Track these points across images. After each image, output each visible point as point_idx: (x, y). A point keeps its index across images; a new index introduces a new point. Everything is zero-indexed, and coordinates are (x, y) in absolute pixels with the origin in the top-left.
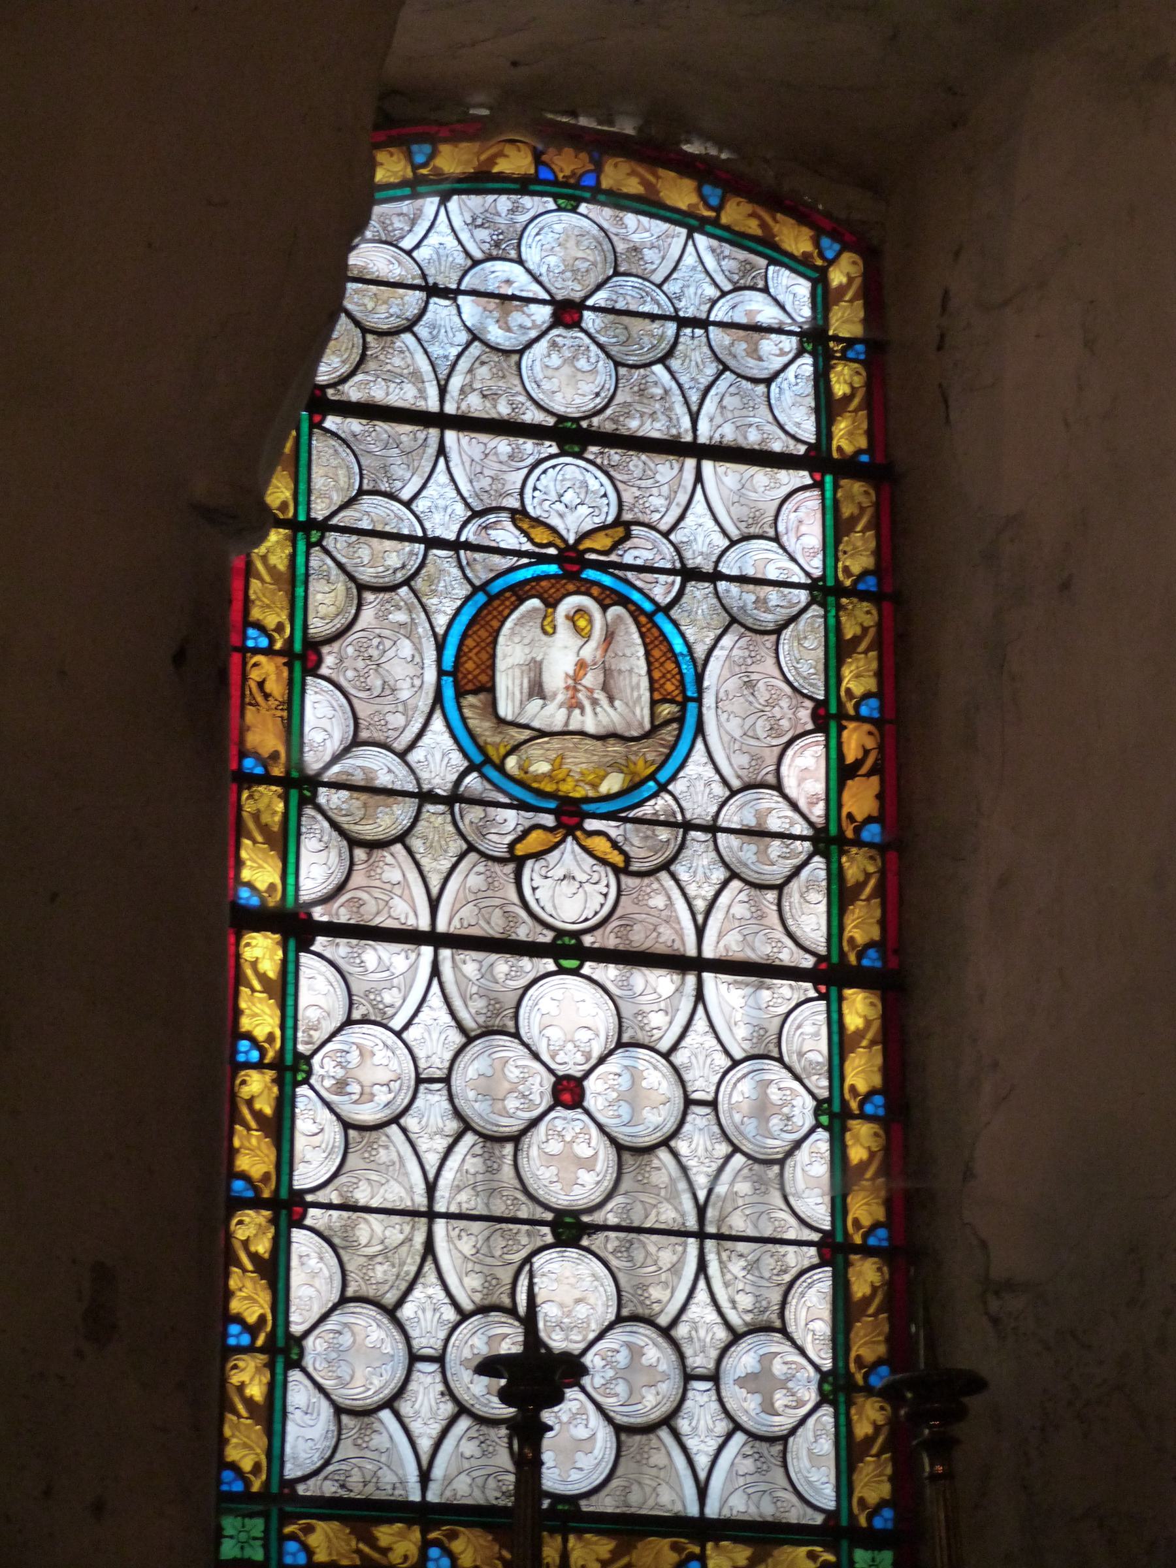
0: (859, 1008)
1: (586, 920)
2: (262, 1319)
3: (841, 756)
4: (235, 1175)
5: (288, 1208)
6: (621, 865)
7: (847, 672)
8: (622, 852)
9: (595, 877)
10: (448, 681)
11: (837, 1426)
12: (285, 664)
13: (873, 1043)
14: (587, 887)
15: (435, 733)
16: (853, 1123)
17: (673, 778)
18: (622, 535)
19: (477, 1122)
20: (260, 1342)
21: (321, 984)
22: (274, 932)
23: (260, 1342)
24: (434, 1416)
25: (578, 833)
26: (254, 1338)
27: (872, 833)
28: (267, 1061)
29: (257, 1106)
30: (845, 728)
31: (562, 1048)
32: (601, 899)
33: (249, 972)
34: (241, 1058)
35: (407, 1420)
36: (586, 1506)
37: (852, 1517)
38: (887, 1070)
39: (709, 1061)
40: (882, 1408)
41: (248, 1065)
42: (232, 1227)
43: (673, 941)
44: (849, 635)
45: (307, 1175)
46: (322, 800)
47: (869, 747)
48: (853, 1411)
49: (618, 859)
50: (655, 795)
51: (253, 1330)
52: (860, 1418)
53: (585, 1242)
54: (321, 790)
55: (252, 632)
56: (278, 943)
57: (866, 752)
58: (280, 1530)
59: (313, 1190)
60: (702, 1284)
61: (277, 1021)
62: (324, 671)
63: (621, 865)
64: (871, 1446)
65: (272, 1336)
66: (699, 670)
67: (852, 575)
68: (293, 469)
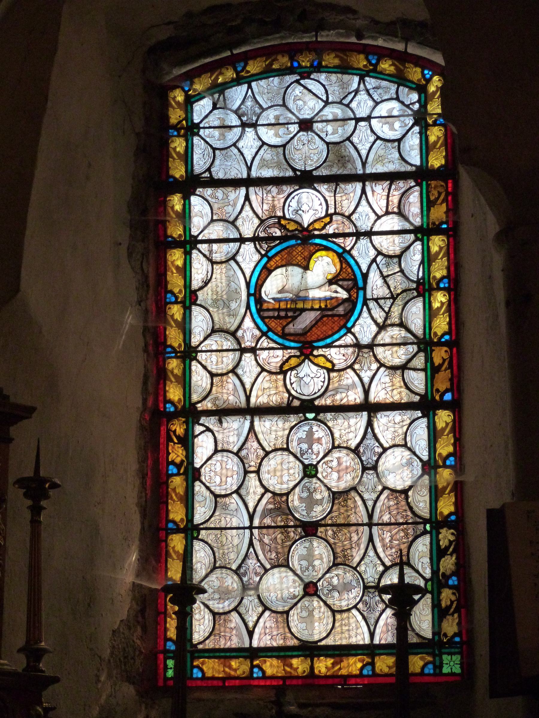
0: (437, 243)
1: (315, 393)
2: (182, 461)
3: (438, 545)
4: (168, 521)
5: (191, 531)
6: (331, 367)
7: (441, 504)
8: (331, 362)
9: (319, 375)
10: (252, 299)
11: (431, 543)
12: (184, 422)
13: (451, 492)
14: (315, 379)
15: (246, 211)
16: (440, 470)
17: (353, 326)
18: (329, 220)
19: (271, 488)
20: (182, 471)
21: (200, 318)
22: (180, 248)
23: (182, 471)
24: (251, 260)
25: (311, 357)
26: (179, 470)
27: (451, 461)
28: (179, 300)
29: (175, 317)
30: (434, 350)
31: (306, 452)
32: (322, 384)
33: (171, 551)
34: (168, 300)
35: (244, 497)
36: (315, 173)
37: (433, 397)
38: (456, 504)
39: (369, 328)
40: (440, 130)
41: (173, 475)
42: (168, 256)
43: (355, 399)
44: (436, 364)
45: (198, 519)
46: (199, 358)
47: (445, 358)
48: (432, 299)
49: (329, 365)
50: (345, 334)
51: (178, 466)
52: (431, 135)
53: (312, 77)
54: (199, 354)
55: (169, 295)
56: (183, 538)
57: (452, 602)
58: (192, 662)
59: (202, 524)
60: (370, 509)
61: (184, 513)
62: (198, 302)
63: (331, 367)
64: (448, 551)
65: (186, 469)
66: (372, 628)
67: (436, 279)
68: (184, 275)
